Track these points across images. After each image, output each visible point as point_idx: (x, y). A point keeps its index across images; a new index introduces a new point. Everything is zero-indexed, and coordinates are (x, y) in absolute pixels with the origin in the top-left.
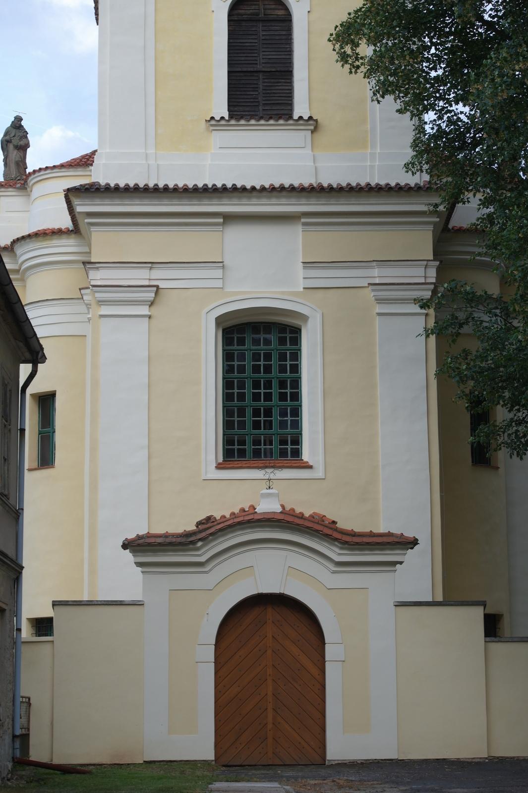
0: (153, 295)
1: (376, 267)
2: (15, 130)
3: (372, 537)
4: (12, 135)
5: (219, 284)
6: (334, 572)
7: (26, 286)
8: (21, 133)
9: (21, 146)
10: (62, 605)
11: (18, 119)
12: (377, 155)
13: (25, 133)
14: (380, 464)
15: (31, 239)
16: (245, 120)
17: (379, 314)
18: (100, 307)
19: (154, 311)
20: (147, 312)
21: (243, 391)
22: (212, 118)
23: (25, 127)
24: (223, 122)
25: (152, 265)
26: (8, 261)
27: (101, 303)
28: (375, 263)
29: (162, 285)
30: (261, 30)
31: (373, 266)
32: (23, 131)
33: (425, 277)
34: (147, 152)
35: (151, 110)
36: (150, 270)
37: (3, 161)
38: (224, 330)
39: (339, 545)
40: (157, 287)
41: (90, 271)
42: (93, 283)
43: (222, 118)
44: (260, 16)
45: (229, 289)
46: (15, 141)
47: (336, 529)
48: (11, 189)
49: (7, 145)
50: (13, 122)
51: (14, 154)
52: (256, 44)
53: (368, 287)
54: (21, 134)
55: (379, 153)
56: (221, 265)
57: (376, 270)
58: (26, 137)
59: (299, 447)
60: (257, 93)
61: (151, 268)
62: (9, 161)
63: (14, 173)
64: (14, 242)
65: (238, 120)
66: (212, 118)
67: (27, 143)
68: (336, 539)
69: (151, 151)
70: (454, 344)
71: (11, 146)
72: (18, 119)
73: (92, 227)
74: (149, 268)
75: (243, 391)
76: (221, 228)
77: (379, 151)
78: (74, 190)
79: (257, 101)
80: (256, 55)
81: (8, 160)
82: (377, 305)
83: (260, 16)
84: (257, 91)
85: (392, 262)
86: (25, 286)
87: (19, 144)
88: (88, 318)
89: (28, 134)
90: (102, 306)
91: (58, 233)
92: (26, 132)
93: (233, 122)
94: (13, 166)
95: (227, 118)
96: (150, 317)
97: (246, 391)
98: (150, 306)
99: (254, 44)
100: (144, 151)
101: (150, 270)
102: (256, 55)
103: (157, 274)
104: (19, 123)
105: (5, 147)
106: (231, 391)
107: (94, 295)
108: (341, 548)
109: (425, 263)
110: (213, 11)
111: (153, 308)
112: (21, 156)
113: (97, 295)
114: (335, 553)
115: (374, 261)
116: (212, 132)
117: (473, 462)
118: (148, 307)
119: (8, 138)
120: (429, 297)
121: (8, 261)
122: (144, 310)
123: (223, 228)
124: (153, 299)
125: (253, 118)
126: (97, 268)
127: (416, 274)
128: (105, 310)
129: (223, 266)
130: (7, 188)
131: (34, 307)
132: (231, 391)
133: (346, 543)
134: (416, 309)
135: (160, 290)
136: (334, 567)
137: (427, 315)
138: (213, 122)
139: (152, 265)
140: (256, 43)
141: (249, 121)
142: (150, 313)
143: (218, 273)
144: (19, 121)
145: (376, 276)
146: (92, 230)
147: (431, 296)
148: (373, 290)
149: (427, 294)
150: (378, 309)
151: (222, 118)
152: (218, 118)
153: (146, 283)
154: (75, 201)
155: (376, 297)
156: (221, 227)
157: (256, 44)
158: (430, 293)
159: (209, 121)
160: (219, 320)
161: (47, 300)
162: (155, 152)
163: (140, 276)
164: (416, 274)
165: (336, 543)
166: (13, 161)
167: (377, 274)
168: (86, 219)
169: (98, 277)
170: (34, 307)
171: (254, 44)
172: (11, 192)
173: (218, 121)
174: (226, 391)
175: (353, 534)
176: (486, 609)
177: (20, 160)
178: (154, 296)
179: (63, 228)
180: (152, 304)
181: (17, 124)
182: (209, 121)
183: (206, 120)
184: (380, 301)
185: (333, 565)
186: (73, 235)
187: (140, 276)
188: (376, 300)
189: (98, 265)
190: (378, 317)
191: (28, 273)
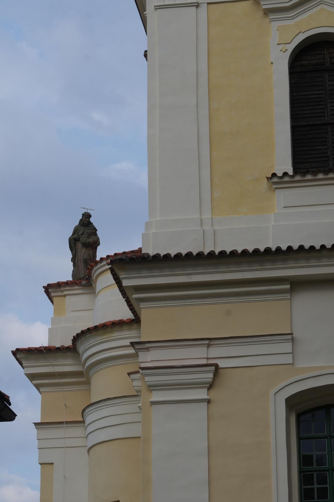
0: (211, 375)
2: (83, 227)
4: (80, 233)
5: (288, 359)
7: (90, 390)
8: (90, 230)
9: (89, 243)
11: (87, 216)
13: (94, 230)
15: (91, 333)
16: (311, 174)
18: (152, 392)
19: (214, 394)
20: (206, 397)
21: (324, 486)
22: (274, 175)
23: (94, 224)
24: (286, 179)
25: (210, 342)
26: (73, 362)
27: (152, 388)
29: (222, 364)
30: (327, 81)
32: (91, 228)
34: (202, 217)
35: (206, 173)
36: (208, 347)
37: (72, 261)
38: (298, 416)
40: (216, 366)
41: (139, 353)
42: (143, 365)
43: (285, 174)
44: (326, 65)
45: (299, 365)
46: (83, 239)
48: (76, 287)
49: (75, 244)
50: (81, 220)
51: (83, 252)
52: (323, 96)
54: (90, 231)
56: (290, 337)
58: (95, 234)
59: (304, 487)
60: (326, 147)
61: (209, 346)
62: (78, 260)
63: (83, 272)
64: (76, 339)
65: (304, 174)
66: (274, 175)
67: (96, 240)
69: (207, 216)
71: (79, 245)
72: (87, 216)
73: (141, 304)
74: (207, 346)
75: (324, 486)
76: (288, 296)
78: (117, 262)
79: (327, 155)
80: (323, 107)
81: (76, 259)
83: (326, 65)
84: (326, 145)
86: (89, 390)
87: (87, 242)
88: (139, 407)
89: (97, 231)
90: (153, 392)
91: (118, 325)
92: (95, 228)
93: (298, 178)
94: (81, 265)
95: (291, 172)
96: (209, 401)
97: (328, 486)
98: (208, 389)
99: (320, 96)
100: (199, 216)
101: (208, 347)
102: (323, 107)
103: (215, 352)
104: (87, 219)
105: (73, 245)
106: (309, 487)
107: (144, 379)
110: (272, 63)
111: (212, 391)
112: (90, 256)
113: (147, 379)
116: (275, 191)
118: (206, 390)
119: (76, 236)
121: (73, 362)
122: (202, 394)
123: (290, 296)
124: (211, 380)
125: (320, 172)
126: (147, 349)
128: (157, 396)
129: (293, 340)
130: (73, 286)
131: (96, 408)
132: (309, 487)
135: (220, 370)
138: (275, 180)
139: (210, 342)
140: (322, 94)
141: (316, 175)
142: (208, 397)
143: (287, 347)
144: (87, 218)
146: (140, 306)
151: (285, 174)
152: (280, 174)
153: (204, 362)
154: (120, 274)
156: (289, 295)
157: (323, 96)
159: (271, 178)
160: (291, 402)
161: (108, 399)
162: (211, 216)
163: (197, 355)
166: (82, 260)
168: (134, 294)
169: (148, 358)
170: (96, 408)
171: (320, 96)
172: (77, 290)
173: (281, 178)
174: (304, 487)
176: (147, 32)
177: (89, 257)
178: (212, 377)
179: (125, 319)
180: (210, 386)
181: (86, 222)
182: (271, 178)
183: (267, 178)
186: (135, 325)
187: (197, 355)
189: (148, 345)
191: (91, 372)
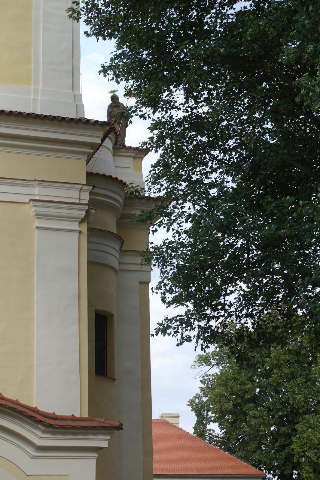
1: (37, 186)
3: (75, 421)
6: (34, 457)
10: (31, 418)
12: (40, 91)
14: (35, 363)
17: (38, 228)
28: (36, 182)
31: (33, 185)
33: (80, 199)
39: (43, 428)
47: (38, 412)
53: (29, 203)
55: (41, 89)
57: (37, 189)
68: (40, 422)
70: (153, 234)
77: (41, 88)
82: (37, 220)
85: (51, 183)
108: (44, 432)
109: (80, 186)
114: (37, 436)
115: (35, 180)
117: (96, 373)
120: (83, 216)
127: (72, 195)
133: (51, 426)
134: (75, 226)
136: (35, 452)
137: (80, 232)
145: (37, 194)
147: (85, 216)
148: (34, 206)
149: (83, 214)
150: (38, 223)
155: (37, 212)
158: (84, 213)
164: (72, 195)
165: (40, 426)
167: (37, 192)
175: (55, 417)
184: (39, 216)
185: (34, 450)
188: (36, 215)
190: (37, 230)
